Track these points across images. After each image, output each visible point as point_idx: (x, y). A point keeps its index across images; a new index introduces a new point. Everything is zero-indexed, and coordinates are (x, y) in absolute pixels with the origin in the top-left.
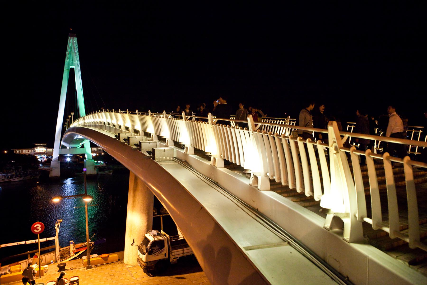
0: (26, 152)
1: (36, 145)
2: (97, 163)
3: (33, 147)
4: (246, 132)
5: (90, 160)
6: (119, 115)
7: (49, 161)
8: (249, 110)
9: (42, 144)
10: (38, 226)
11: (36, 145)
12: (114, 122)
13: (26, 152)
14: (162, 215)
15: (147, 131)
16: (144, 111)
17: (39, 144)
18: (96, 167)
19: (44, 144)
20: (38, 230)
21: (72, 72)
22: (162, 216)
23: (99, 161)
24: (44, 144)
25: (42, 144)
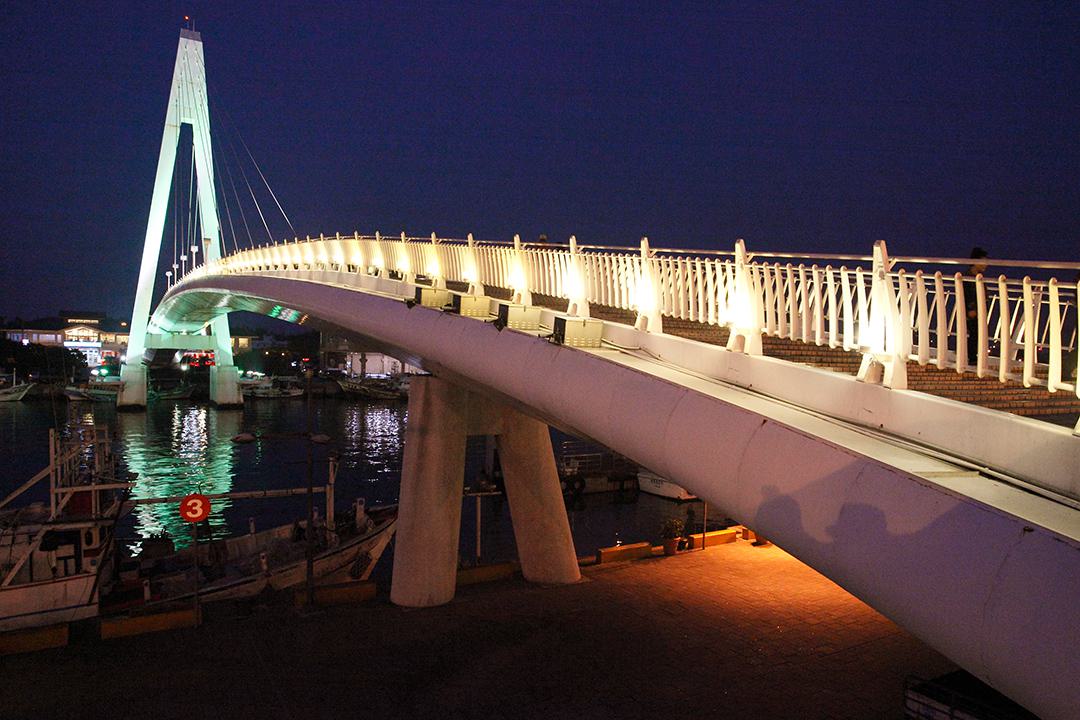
0: (47, 338)
1: (69, 321)
2: (244, 375)
3: (59, 325)
4: (512, 251)
5: (228, 369)
6: (321, 244)
7: (114, 366)
8: (201, 500)
9: (85, 321)
10: (195, 504)
11: (69, 321)
12: (324, 259)
13: (47, 338)
14: (480, 494)
15: (463, 278)
16: (391, 234)
17: (77, 321)
18: (242, 386)
19: (93, 321)
20: (195, 512)
21: (186, 131)
22: (482, 496)
23: (250, 373)
24: (93, 321)
25: (85, 321)
